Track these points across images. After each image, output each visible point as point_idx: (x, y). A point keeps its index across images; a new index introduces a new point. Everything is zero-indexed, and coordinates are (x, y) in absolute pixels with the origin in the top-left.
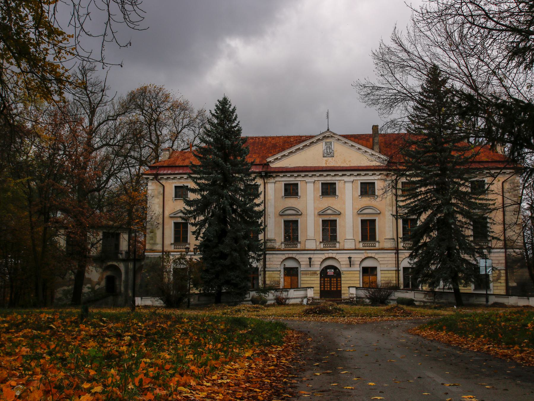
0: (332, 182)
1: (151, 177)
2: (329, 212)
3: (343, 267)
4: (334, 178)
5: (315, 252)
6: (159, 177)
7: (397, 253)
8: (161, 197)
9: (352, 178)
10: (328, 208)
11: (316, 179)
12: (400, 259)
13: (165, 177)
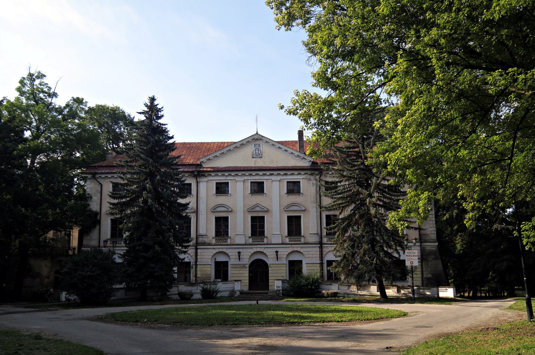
0: (261, 181)
1: (89, 176)
2: (258, 209)
3: (270, 261)
4: (262, 178)
5: (244, 246)
6: (97, 176)
7: (321, 248)
8: (99, 195)
9: (279, 178)
10: (257, 205)
11: (246, 178)
12: (324, 253)
13: (103, 176)
